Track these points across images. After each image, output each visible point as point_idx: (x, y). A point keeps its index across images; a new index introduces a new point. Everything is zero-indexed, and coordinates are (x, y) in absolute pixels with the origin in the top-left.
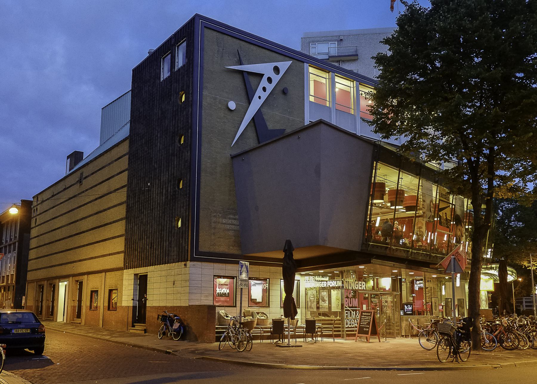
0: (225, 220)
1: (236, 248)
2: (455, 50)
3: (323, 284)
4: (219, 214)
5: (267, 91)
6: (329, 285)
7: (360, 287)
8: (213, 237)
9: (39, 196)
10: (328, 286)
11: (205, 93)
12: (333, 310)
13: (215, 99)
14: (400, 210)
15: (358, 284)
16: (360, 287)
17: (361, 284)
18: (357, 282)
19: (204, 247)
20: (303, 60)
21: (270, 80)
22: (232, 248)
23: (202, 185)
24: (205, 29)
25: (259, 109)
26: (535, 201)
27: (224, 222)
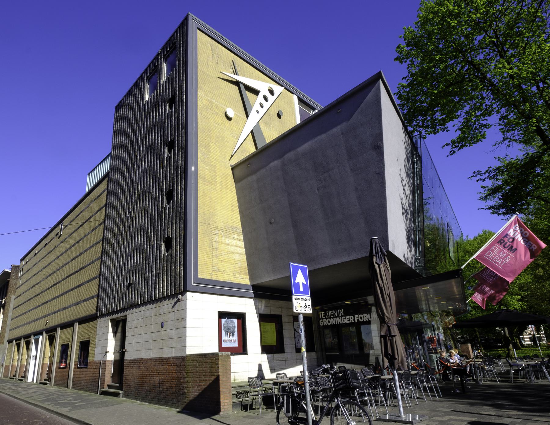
0: (228, 241)
1: (535, 200)
2: (531, 34)
3: (349, 319)
4: (221, 232)
5: (274, 95)
6: (358, 320)
7: (348, 321)
8: (215, 261)
9: (22, 278)
10: (356, 321)
11: (200, 93)
13: (211, 102)
15: (345, 318)
16: (348, 321)
17: (349, 318)
18: (344, 317)
19: (294, 322)
20: (293, 92)
21: (266, 99)
22: (238, 275)
23: (200, 194)
24: (198, 31)
25: (258, 124)
26: (549, 227)
27: (227, 242)
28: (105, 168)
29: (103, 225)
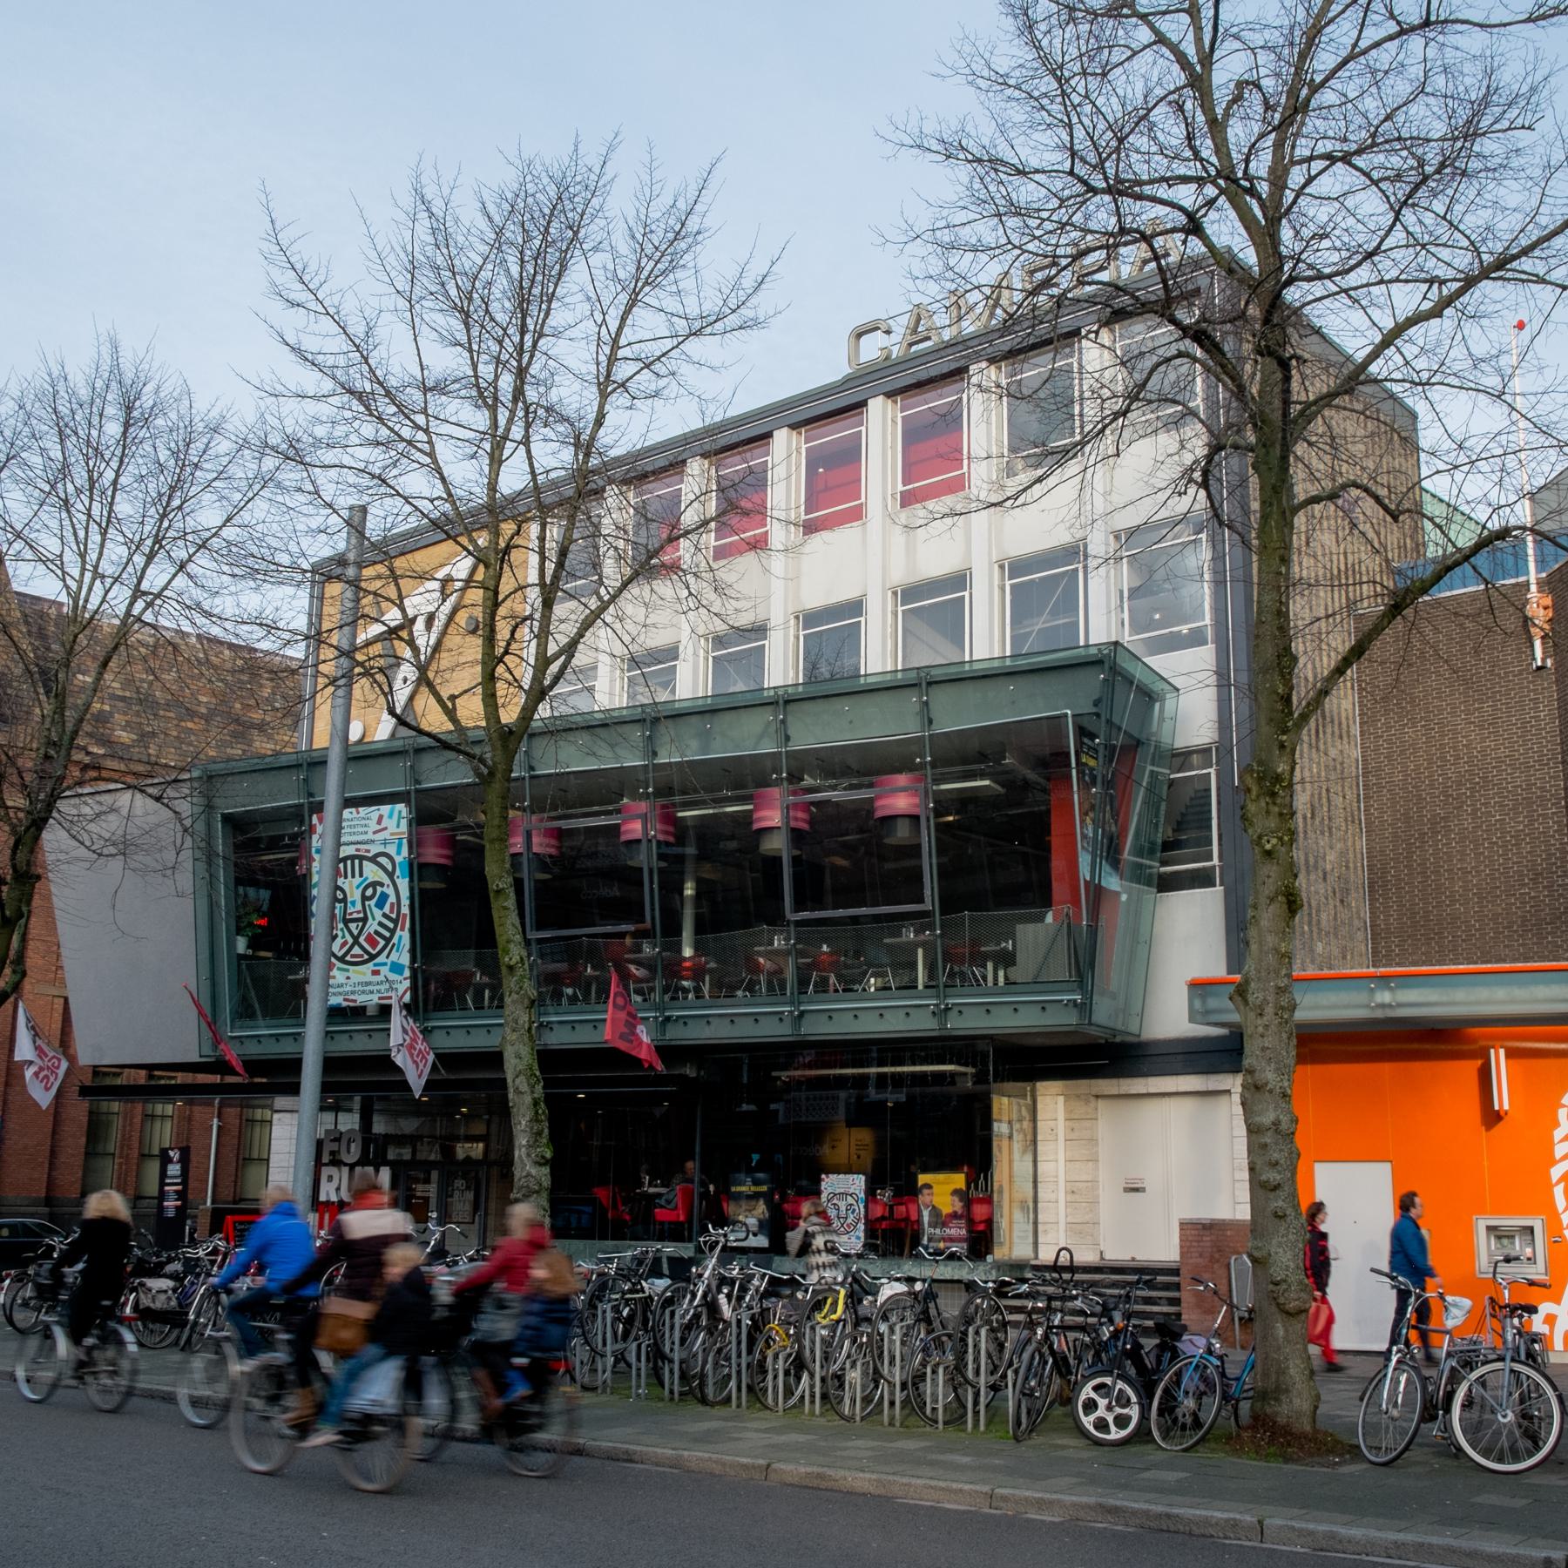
12: (73, 752)
14: (1162, 192)
28: (1057, 1519)
29: (1352, 293)
